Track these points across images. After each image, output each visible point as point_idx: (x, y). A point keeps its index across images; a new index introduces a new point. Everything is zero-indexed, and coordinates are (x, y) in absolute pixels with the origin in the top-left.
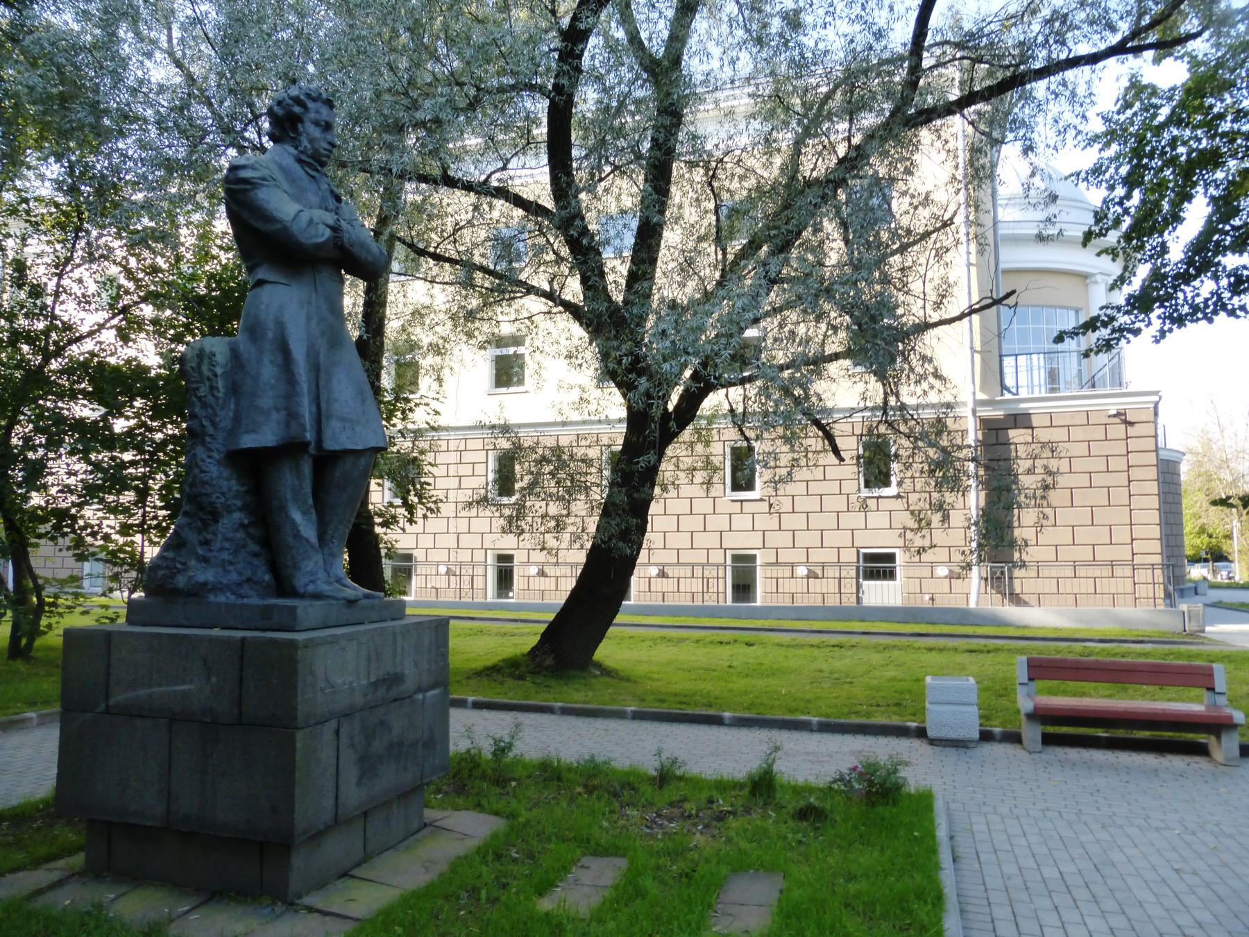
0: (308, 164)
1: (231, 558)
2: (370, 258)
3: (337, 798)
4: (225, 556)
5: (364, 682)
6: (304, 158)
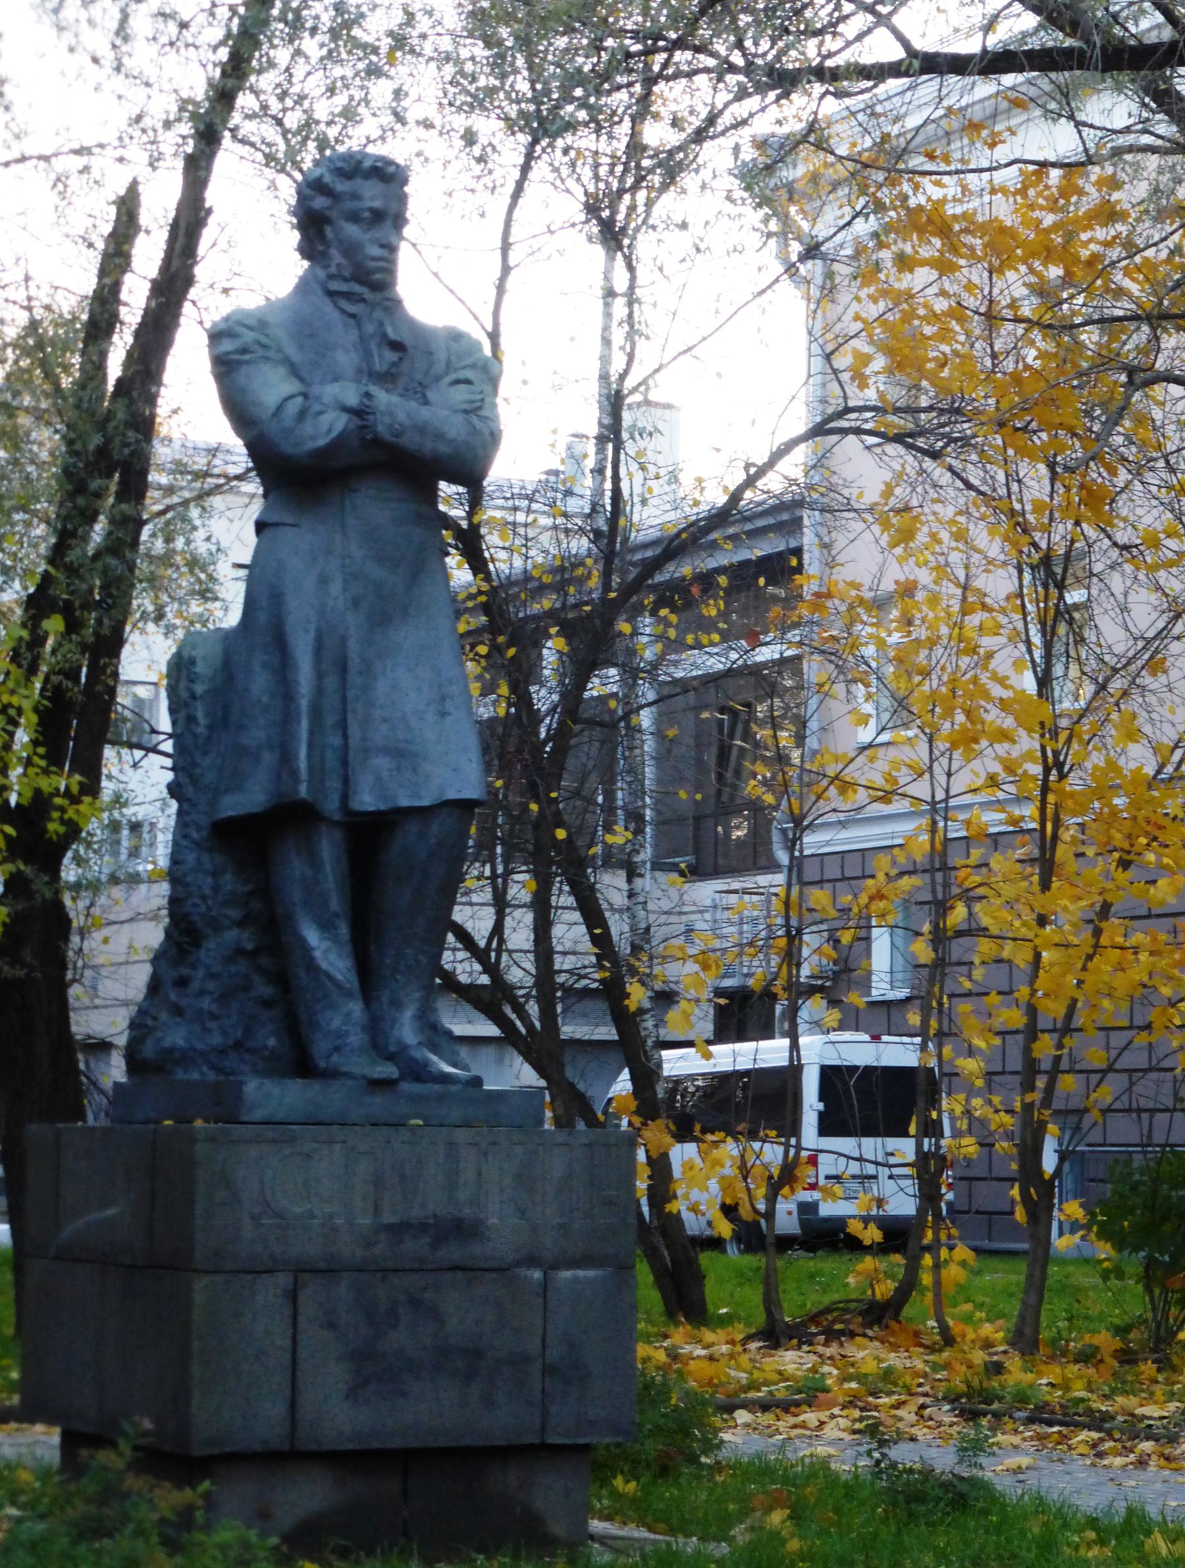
0: (347, 295)
1: (214, 1008)
2: (443, 449)
3: (293, 1405)
4: (206, 1003)
5: (365, 1221)
6: (335, 286)
